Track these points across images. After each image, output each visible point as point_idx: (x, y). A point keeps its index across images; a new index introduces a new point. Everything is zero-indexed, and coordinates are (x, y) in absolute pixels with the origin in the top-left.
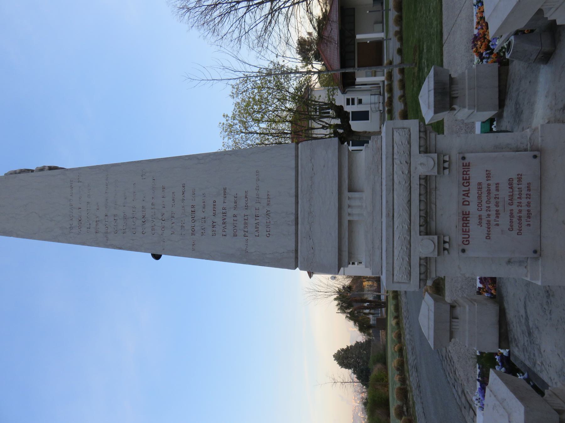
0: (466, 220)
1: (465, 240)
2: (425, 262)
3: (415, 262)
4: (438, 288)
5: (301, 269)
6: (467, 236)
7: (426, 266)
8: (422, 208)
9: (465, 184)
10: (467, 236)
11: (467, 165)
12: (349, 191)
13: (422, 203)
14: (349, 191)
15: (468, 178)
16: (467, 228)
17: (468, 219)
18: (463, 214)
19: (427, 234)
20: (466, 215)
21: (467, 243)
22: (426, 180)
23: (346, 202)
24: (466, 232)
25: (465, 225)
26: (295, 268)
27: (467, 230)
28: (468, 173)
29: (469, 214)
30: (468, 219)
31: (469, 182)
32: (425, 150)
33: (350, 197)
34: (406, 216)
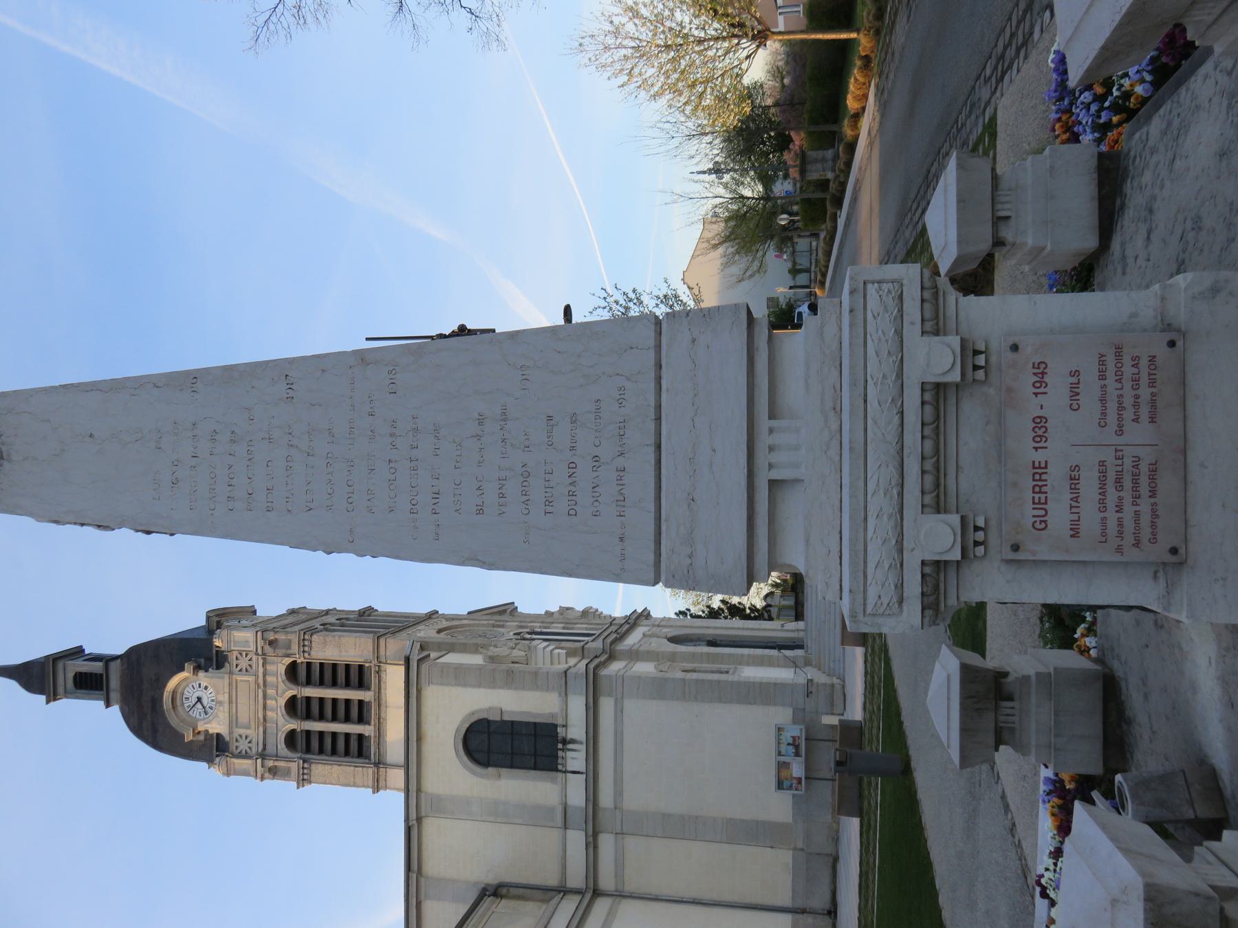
0: (1040, 480)
1: (1038, 519)
2: (935, 571)
3: (913, 398)
4: (969, 629)
5: (667, 585)
6: (1043, 512)
7: (937, 409)
8: (928, 315)
9: (1038, 525)
10: (1043, 512)
11: (1043, 465)
12: (770, 418)
13: (928, 408)
14: (770, 418)
15: (1043, 501)
16: (1043, 496)
17: (1044, 477)
18: (1034, 468)
19: (937, 333)
20: (1040, 467)
21: (1043, 525)
22: (937, 392)
23: (763, 440)
24: (1039, 503)
25: (1037, 489)
26: (655, 584)
27: (1043, 501)
28: (1044, 489)
29: (1046, 467)
30: (1044, 477)
31: (1045, 522)
32: (935, 326)
33: (773, 461)
34: (892, 471)
